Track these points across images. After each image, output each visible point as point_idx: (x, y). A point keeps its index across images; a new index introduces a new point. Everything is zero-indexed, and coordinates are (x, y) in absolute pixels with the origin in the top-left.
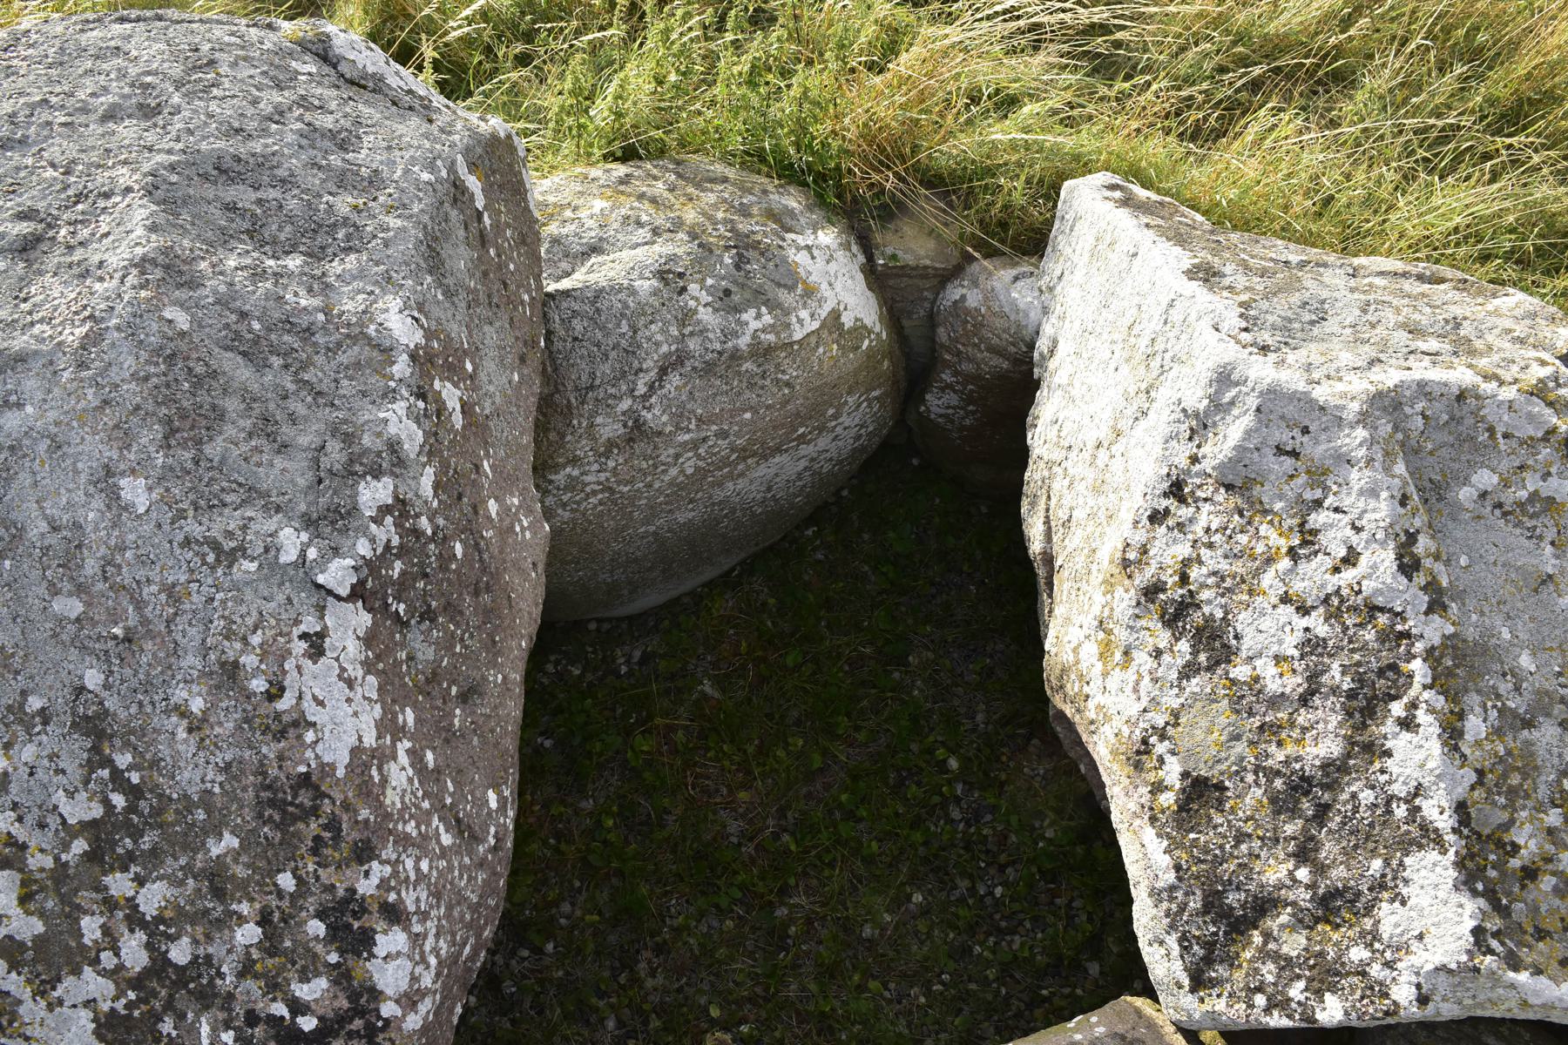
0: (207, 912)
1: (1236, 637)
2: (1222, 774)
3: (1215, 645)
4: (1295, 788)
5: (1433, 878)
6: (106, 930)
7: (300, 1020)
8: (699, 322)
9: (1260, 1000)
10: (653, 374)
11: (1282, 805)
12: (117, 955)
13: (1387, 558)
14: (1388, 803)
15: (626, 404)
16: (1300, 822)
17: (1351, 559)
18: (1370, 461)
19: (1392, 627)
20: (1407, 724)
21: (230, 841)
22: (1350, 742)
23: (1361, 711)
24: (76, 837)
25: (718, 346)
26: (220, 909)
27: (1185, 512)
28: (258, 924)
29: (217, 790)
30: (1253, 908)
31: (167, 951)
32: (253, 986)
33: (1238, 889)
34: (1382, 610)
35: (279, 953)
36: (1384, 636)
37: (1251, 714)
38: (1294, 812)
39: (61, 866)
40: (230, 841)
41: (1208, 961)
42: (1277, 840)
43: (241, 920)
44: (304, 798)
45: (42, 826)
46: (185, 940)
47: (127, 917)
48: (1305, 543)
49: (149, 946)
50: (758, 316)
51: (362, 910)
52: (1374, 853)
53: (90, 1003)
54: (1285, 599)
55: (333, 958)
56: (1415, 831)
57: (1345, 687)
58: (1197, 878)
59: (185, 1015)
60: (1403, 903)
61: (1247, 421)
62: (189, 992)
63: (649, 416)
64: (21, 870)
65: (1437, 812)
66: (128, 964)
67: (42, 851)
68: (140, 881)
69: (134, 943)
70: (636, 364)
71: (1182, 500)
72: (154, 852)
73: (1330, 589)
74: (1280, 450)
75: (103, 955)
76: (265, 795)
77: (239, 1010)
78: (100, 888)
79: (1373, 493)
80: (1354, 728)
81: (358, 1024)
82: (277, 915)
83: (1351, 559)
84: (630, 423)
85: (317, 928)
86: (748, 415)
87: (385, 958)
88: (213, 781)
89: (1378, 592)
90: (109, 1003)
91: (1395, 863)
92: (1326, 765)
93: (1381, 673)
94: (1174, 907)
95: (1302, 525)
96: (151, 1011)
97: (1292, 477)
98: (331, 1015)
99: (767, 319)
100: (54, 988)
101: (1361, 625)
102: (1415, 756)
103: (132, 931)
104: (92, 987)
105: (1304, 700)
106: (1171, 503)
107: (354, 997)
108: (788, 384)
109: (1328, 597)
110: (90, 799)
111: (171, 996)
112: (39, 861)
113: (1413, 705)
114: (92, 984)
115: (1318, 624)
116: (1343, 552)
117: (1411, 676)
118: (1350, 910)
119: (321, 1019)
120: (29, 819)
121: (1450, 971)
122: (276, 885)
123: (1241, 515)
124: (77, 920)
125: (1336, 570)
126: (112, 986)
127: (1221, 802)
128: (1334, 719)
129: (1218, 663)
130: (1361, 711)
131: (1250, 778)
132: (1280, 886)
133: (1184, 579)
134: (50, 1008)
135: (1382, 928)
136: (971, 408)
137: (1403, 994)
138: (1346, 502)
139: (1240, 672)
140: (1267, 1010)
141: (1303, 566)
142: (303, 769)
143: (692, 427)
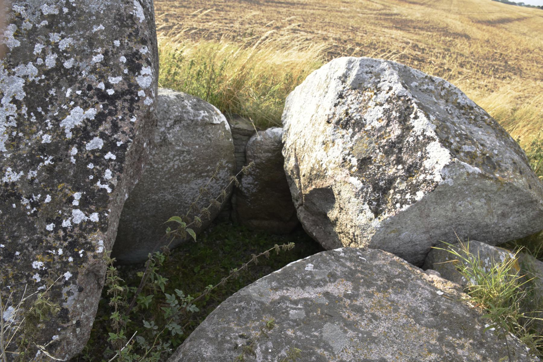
0: (84, 50)
1: (365, 120)
2: (369, 154)
3: (359, 124)
4: (391, 147)
5: (435, 148)
6: (44, 51)
7: (108, 91)
8: (187, 109)
9: (398, 205)
10: (172, 121)
11: (387, 153)
12: (44, 61)
13: (400, 86)
14: (417, 138)
15: (163, 129)
16: (395, 155)
17: (391, 88)
18: (389, 68)
19: (405, 99)
20: (416, 118)
21: (102, 27)
22: (402, 129)
23: (403, 121)
24: (44, 20)
25: (192, 118)
26: (89, 51)
27: (344, 100)
28: (103, 54)
29: (102, 12)
30: (388, 184)
31: (63, 63)
32: (94, 77)
33: (382, 180)
34: (401, 96)
35: (108, 65)
36: (403, 102)
37: (374, 136)
38: (393, 153)
39: (34, 27)
40: (102, 27)
41: (378, 205)
42: (390, 164)
43: (96, 54)
44: (129, 22)
45: (33, 14)
46: (72, 59)
47: (53, 49)
48: (378, 91)
49: (57, 60)
50: (204, 113)
51: (140, 58)
52: (417, 151)
53: (25, 77)
54: (376, 105)
55: (126, 71)
56: (426, 140)
57: (398, 115)
58: (369, 182)
59: (61, 88)
60: (429, 158)
61: (358, 68)
62: (67, 78)
63: (169, 136)
64: (18, 27)
65: (430, 133)
66: (47, 65)
67: (30, 22)
68: (63, 37)
69: (52, 57)
70: (168, 116)
71: (342, 98)
72: (72, 29)
73: (387, 97)
74: (367, 73)
75: (39, 60)
76: (117, 17)
77: (86, 84)
78: (47, 37)
79: (392, 74)
80: (403, 125)
81: (128, 97)
82: (111, 53)
83: (391, 88)
84: (162, 138)
85: (123, 59)
86: (197, 147)
87: (144, 75)
88: (102, 9)
89: (399, 92)
90: (33, 78)
91: (424, 150)
92: (398, 137)
93: (405, 110)
94: (364, 194)
95: (376, 87)
96: (48, 84)
97: (371, 78)
98: (120, 90)
99: (207, 114)
100: (14, 68)
101: (398, 101)
102: (421, 124)
103: (53, 53)
104: (29, 70)
105: (388, 125)
106: (340, 100)
107: (130, 85)
108: (210, 139)
109: (387, 99)
110: (55, 8)
111: (59, 79)
112: (27, 25)
113: (416, 113)
114: (31, 69)
115: (386, 106)
116: (388, 88)
117: (413, 107)
118: (416, 170)
119: (116, 91)
120: (29, 11)
121: (448, 165)
122: (113, 43)
123: (360, 93)
124: (34, 44)
125: (388, 93)
126: (37, 71)
127: (370, 162)
128: (397, 125)
129: (361, 129)
130: (403, 121)
131: (378, 151)
132: (394, 174)
133: (347, 114)
134: (9, 75)
135: (426, 167)
136: (256, 183)
137: (438, 178)
138: (386, 79)
139: (368, 128)
140: (401, 207)
141: (379, 96)
142: (132, 13)
143: (181, 145)
